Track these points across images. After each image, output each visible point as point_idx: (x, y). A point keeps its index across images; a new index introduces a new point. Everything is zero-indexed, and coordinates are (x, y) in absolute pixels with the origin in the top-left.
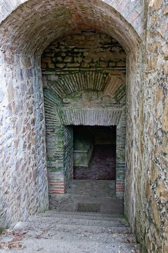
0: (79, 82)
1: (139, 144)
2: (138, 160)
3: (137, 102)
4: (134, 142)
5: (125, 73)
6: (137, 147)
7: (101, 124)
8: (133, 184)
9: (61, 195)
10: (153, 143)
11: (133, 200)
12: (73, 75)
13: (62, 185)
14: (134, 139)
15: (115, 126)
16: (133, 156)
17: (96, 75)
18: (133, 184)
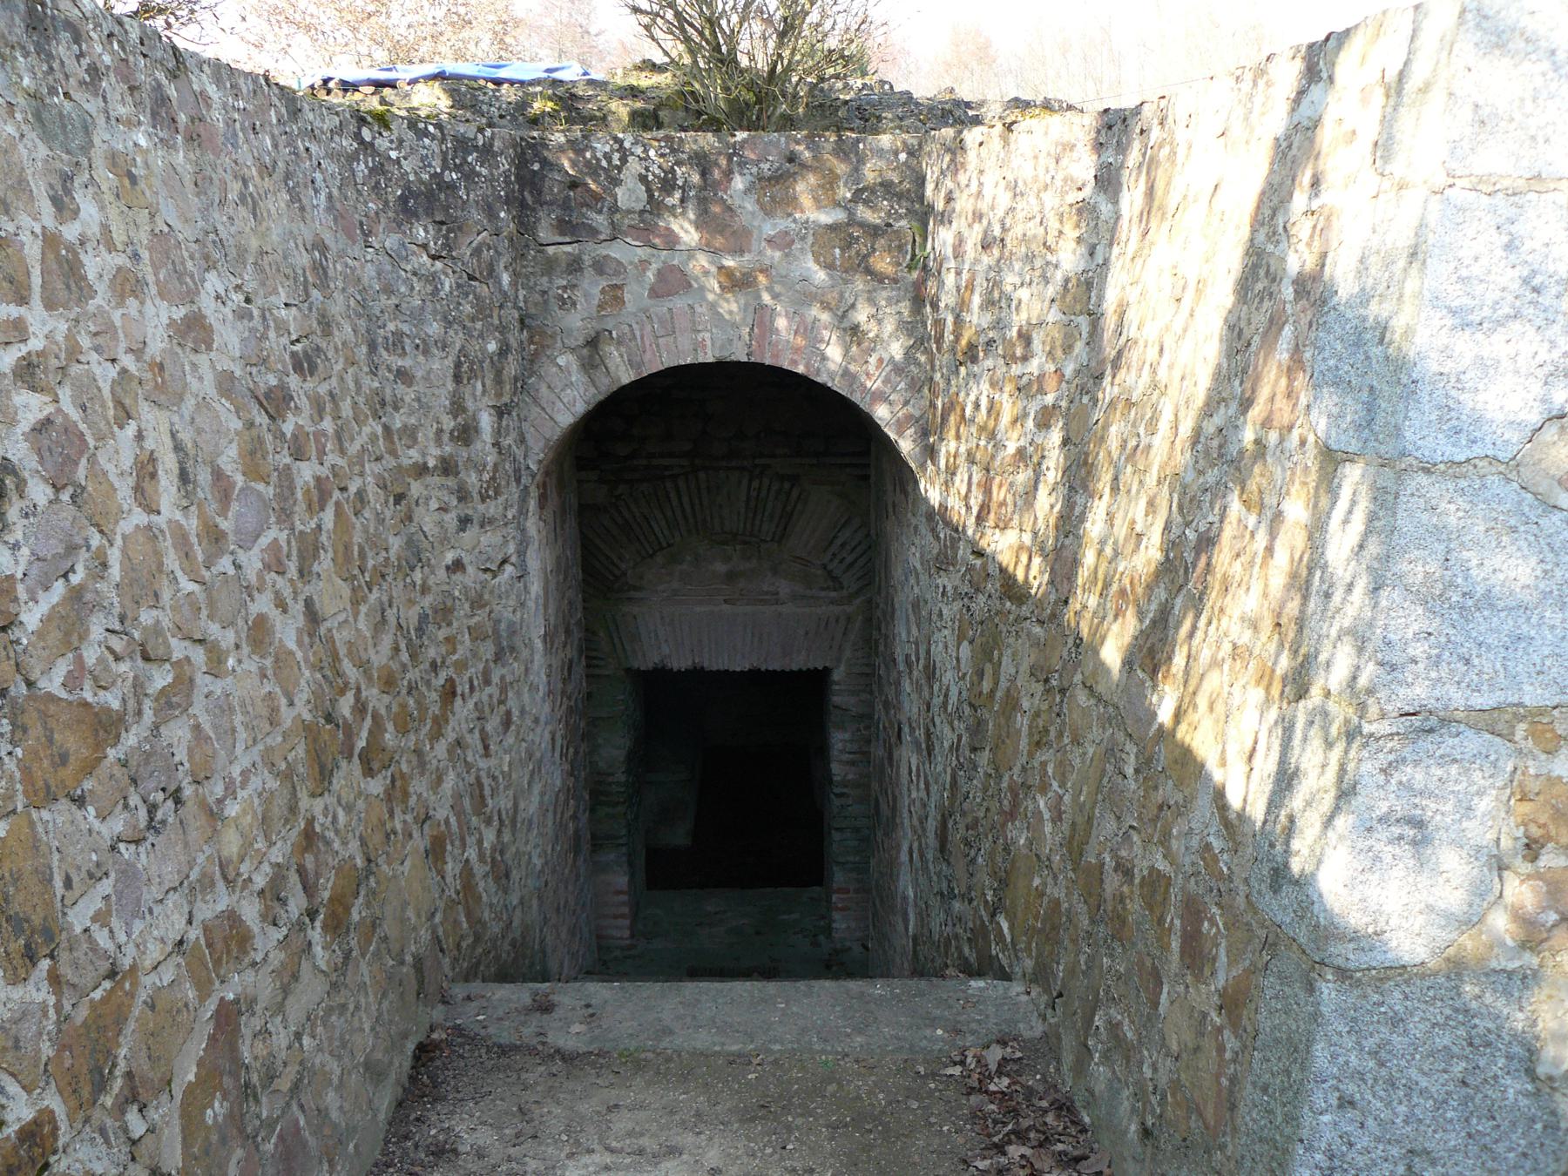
0: (688, 510)
1: (920, 734)
2: (918, 776)
3: (912, 617)
4: (906, 729)
5: (866, 478)
6: (917, 744)
7: (775, 666)
8: (905, 848)
9: (620, 930)
10: (761, 110)
11: (905, 898)
12: (669, 485)
13: (623, 903)
14: (904, 720)
15: (826, 672)
16: (904, 771)
17: (755, 484)
18: (905, 848)
